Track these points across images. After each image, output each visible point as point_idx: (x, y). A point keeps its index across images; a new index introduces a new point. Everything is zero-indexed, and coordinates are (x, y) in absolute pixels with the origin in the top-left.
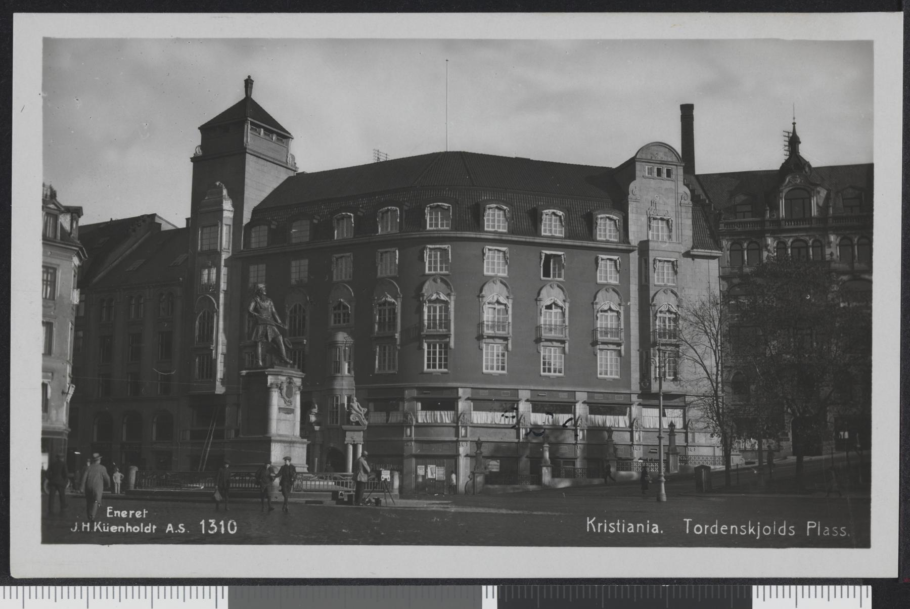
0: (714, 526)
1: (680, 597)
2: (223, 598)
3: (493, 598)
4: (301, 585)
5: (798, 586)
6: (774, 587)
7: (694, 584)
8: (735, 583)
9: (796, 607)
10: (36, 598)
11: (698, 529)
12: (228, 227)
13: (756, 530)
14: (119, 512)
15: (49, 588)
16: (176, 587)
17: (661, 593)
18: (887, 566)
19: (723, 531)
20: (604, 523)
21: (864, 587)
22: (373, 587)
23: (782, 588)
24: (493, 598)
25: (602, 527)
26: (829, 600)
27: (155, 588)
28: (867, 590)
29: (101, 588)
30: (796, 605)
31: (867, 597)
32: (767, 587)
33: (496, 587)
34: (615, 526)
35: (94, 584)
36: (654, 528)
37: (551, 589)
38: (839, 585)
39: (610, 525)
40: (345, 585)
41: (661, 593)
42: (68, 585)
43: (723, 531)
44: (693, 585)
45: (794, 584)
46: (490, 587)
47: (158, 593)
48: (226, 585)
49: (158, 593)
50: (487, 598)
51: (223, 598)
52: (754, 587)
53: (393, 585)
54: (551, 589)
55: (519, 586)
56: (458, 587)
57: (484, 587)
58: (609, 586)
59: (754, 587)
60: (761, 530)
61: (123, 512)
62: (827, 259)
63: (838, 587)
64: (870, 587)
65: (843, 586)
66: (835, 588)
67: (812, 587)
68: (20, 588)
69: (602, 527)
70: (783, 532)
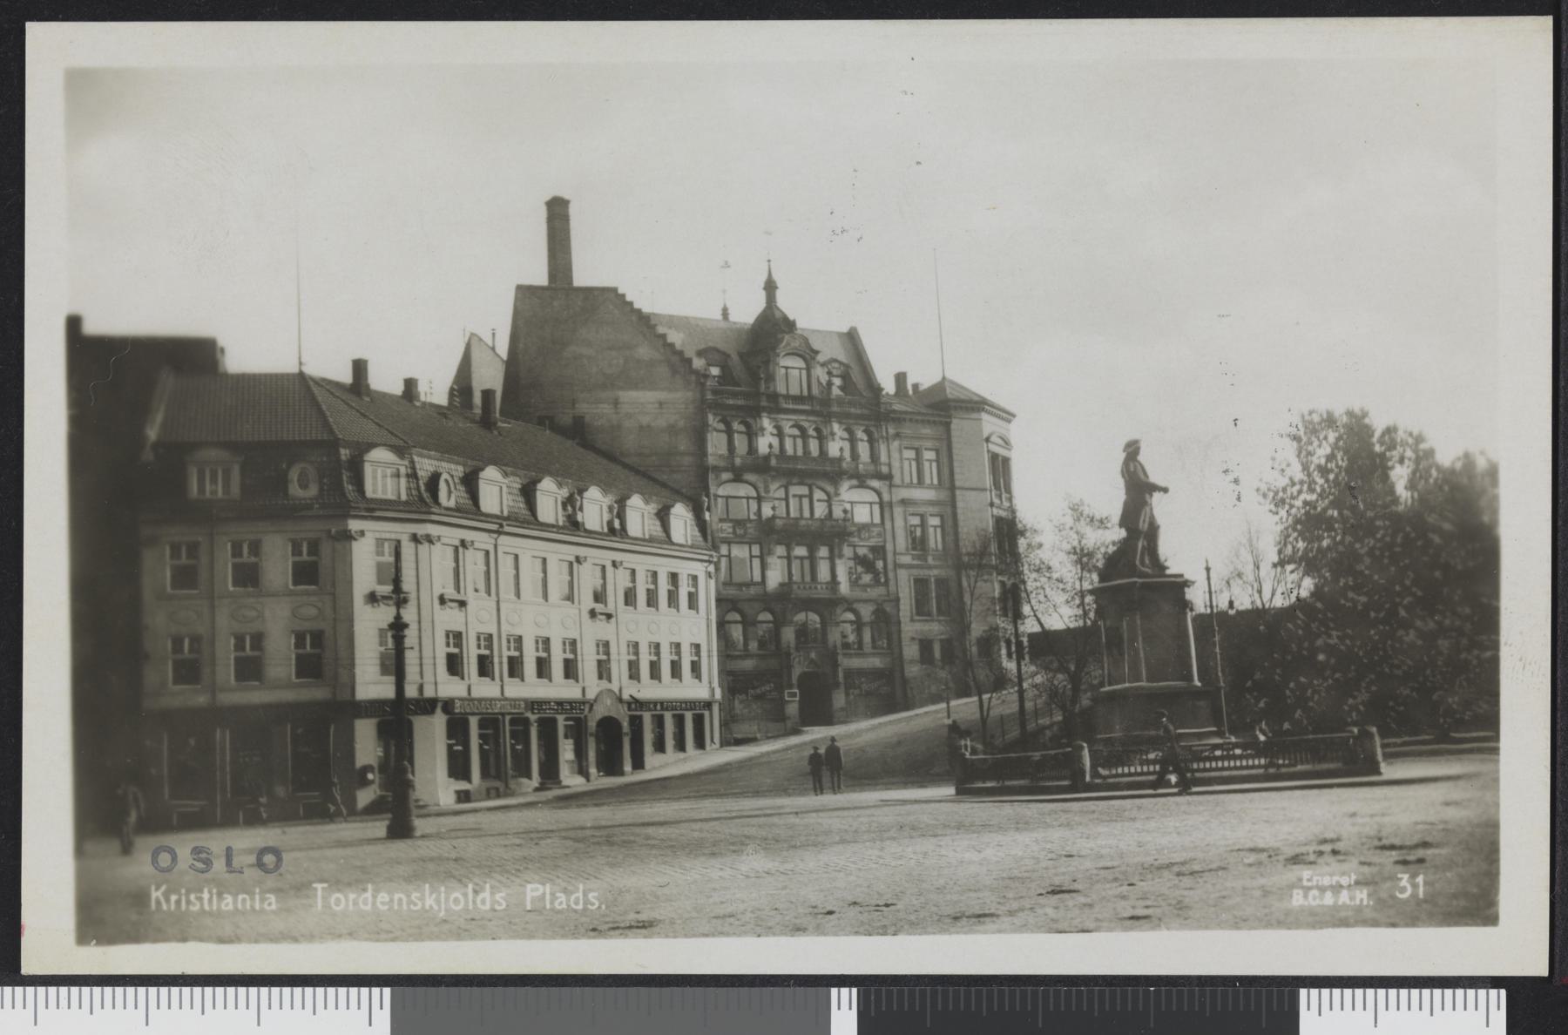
0: (577, 895)
1: (951, 1008)
2: (381, 1008)
3: (850, 1008)
4: (427, 986)
5: (1379, 990)
6: (1336, 992)
7: (1198, 986)
8: (1269, 985)
9: (1376, 1026)
10: (58, 1008)
11: (456, 901)
12: (797, 499)
13: (438, 901)
14: (1320, 878)
15: (91, 990)
16: (300, 989)
17: (1119, 1001)
18: (1536, 964)
19: (382, 903)
20: (180, 895)
21: (1493, 992)
22: (676, 989)
23: (267, 992)
24: (850, 1008)
25: (178, 902)
26: (1320, 1015)
27: (264, 990)
28: (1499, 997)
29: (147, 991)
30: (1376, 1022)
31: (1499, 1009)
32: (320, 990)
33: (855, 990)
34: (200, 899)
35: (80, 985)
36: (560, 900)
37: (951, 994)
38: (99, 986)
39: (413, 897)
40: (593, 986)
41: (1119, 1001)
42: (113, 986)
43: (382, 903)
44: (1197, 988)
45: (1371, 986)
46: (845, 991)
47: (270, 999)
48: (387, 986)
49: (270, 999)
50: (839, 1008)
51: (381, 1008)
52: (1303, 992)
53: (678, 986)
54: (951, 994)
55: (895, 989)
56: (800, 990)
57: (834, 991)
58: (1052, 989)
59: (1303, 992)
60: (447, 899)
61: (240, 897)
62: (788, 454)
63: (1449, 992)
64: (1503, 992)
65: (1457, 990)
66: (303, 992)
67: (1404, 992)
68: (30, 990)
69: (178, 902)
70: (366, 904)
